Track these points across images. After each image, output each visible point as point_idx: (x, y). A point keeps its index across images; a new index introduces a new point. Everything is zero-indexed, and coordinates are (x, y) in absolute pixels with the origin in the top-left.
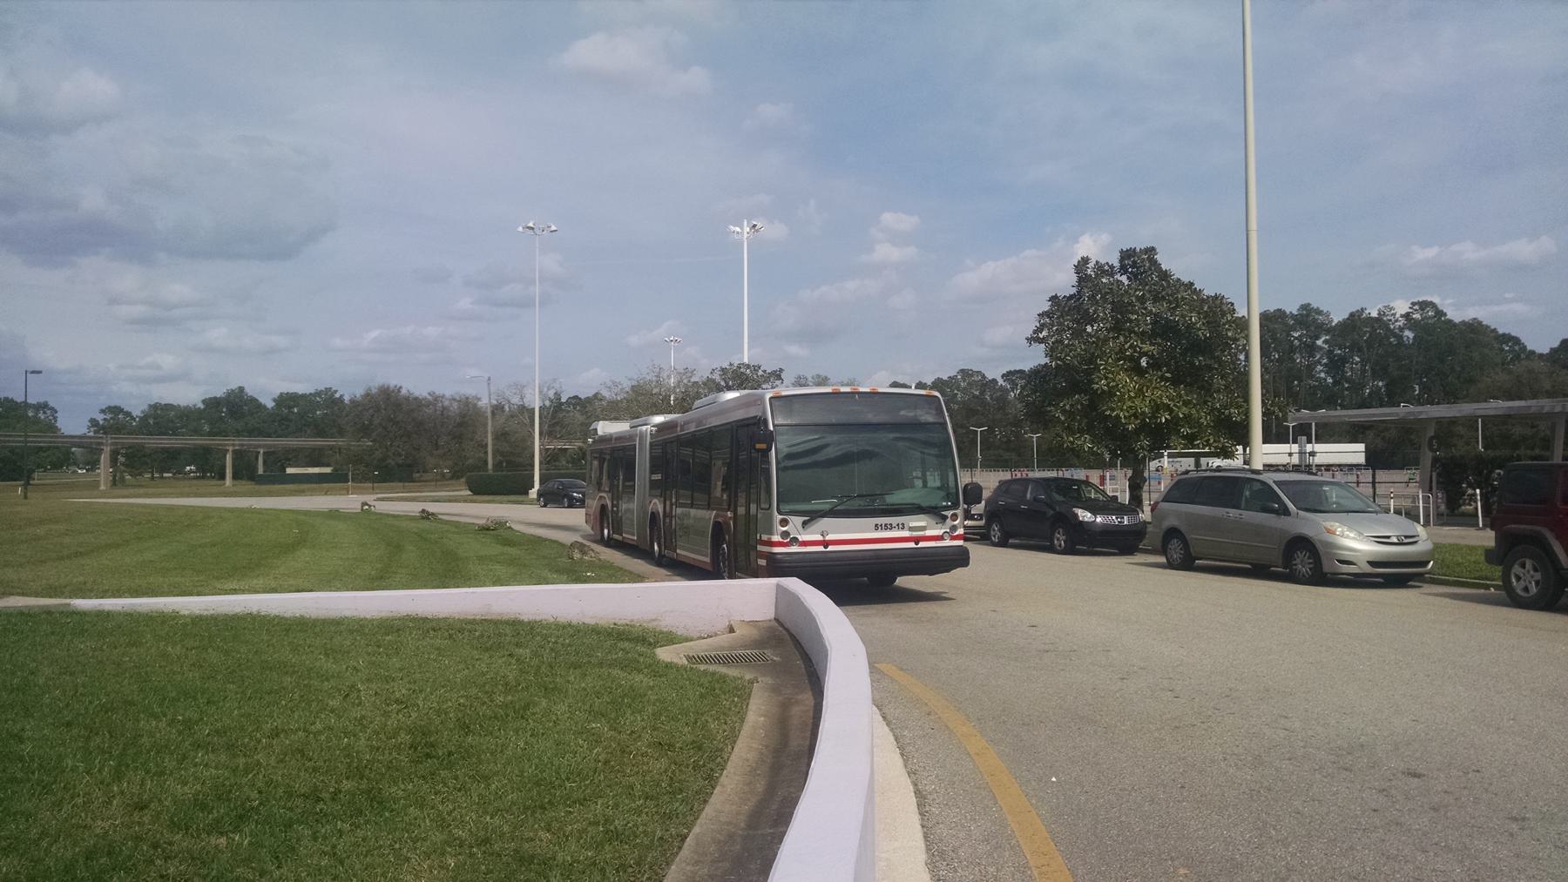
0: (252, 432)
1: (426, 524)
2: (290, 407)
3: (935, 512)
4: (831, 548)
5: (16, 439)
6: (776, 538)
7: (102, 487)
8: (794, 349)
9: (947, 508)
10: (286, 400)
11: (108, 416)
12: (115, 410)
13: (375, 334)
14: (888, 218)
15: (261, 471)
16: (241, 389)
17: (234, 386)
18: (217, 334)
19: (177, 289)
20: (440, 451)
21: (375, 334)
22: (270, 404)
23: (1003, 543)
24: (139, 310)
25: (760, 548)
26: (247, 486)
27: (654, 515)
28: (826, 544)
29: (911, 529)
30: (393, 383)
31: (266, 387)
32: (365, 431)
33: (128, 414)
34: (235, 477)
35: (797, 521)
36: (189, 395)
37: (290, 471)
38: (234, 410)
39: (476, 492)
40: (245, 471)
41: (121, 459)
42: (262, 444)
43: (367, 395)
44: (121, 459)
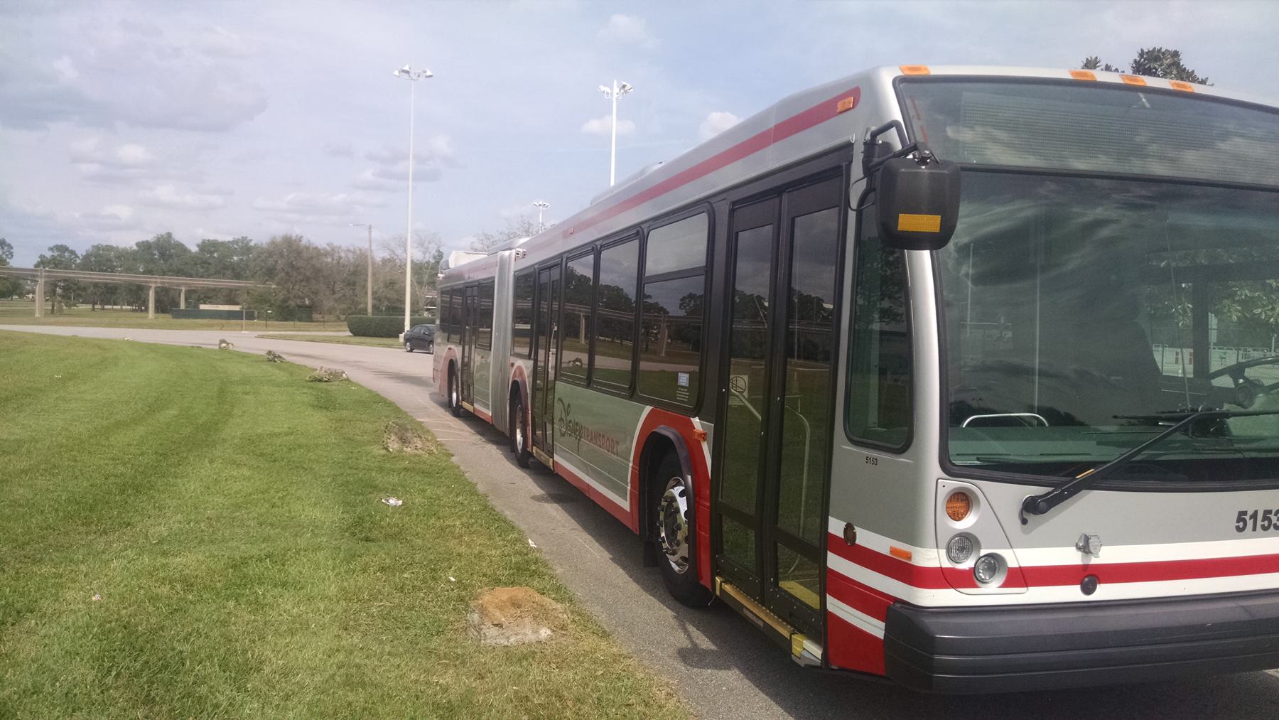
0: (179, 272)
1: (267, 368)
2: (211, 253)
4: (1105, 592)
6: (930, 557)
7: (37, 315)
10: (208, 247)
11: (56, 254)
12: (62, 249)
13: (291, 196)
15: (183, 306)
16: (169, 235)
17: (163, 232)
18: (165, 192)
19: (132, 152)
20: (337, 296)
21: (291, 196)
22: (194, 249)
25: (836, 562)
27: (516, 387)
30: (296, 232)
31: (191, 236)
32: (270, 273)
33: (73, 252)
35: (1005, 497)
36: (127, 241)
37: (202, 307)
38: (163, 253)
39: (356, 332)
40: (166, 305)
41: (59, 291)
42: (183, 284)
43: (273, 243)
44: (59, 291)
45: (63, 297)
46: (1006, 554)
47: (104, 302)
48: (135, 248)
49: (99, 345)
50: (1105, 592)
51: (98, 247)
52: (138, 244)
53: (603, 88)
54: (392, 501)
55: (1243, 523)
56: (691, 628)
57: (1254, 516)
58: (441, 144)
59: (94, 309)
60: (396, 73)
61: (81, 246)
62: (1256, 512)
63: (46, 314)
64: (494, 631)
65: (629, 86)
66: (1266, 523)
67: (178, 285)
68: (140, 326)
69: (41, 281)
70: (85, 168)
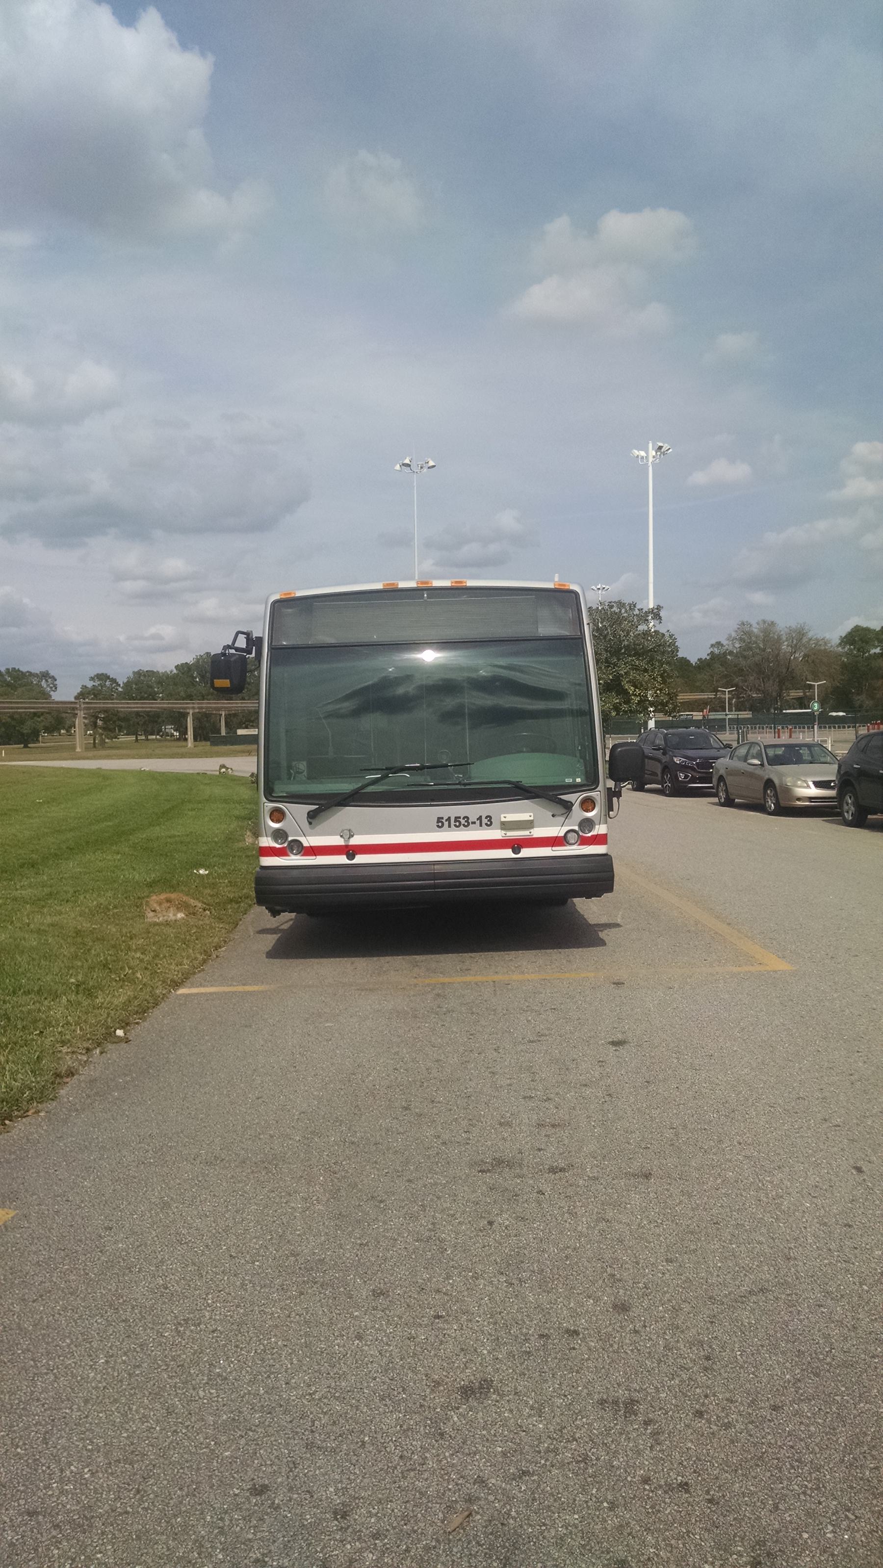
3: (551, 795)
4: (360, 859)
5: (18, 704)
6: (266, 841)
7: (78, 750)
8: (758, 597)
9: (574, 788)
11: (97, 683)
14: (861, 448)
15: (223, 733)
18: (209, 605)
19: (174, 565)
23: (859, 822)
24: (139, 585)
26: (206, 746)
28: (351, 851)
29: (505, 826)
33: (114, 681)
34: (195, 739)
35: (298, 812)
37: (240, 732)
41: (100, 723)
45: (104, 729)
46: (302, 839)
47: (147, 733)
48: (175, 671)
49: (98, 773)
50: (360, 859)
51: (139, 674)
52: (177, 667)
53: (636, 452)
54: (202, 872)
55: (440, 823)
56: (291, 923)
57: (449, 819)
58: (508, 520)
59: (137, 740)
60: (398, 467)
61: (122, 674)
62: (449, 818)
63: (87, 749)
64: (152, 914)
65: (666, 446)
66: (457, 824)
67: (219, 709)
68: (182, 756)
69: (81, 714)
70: (129, 586)
